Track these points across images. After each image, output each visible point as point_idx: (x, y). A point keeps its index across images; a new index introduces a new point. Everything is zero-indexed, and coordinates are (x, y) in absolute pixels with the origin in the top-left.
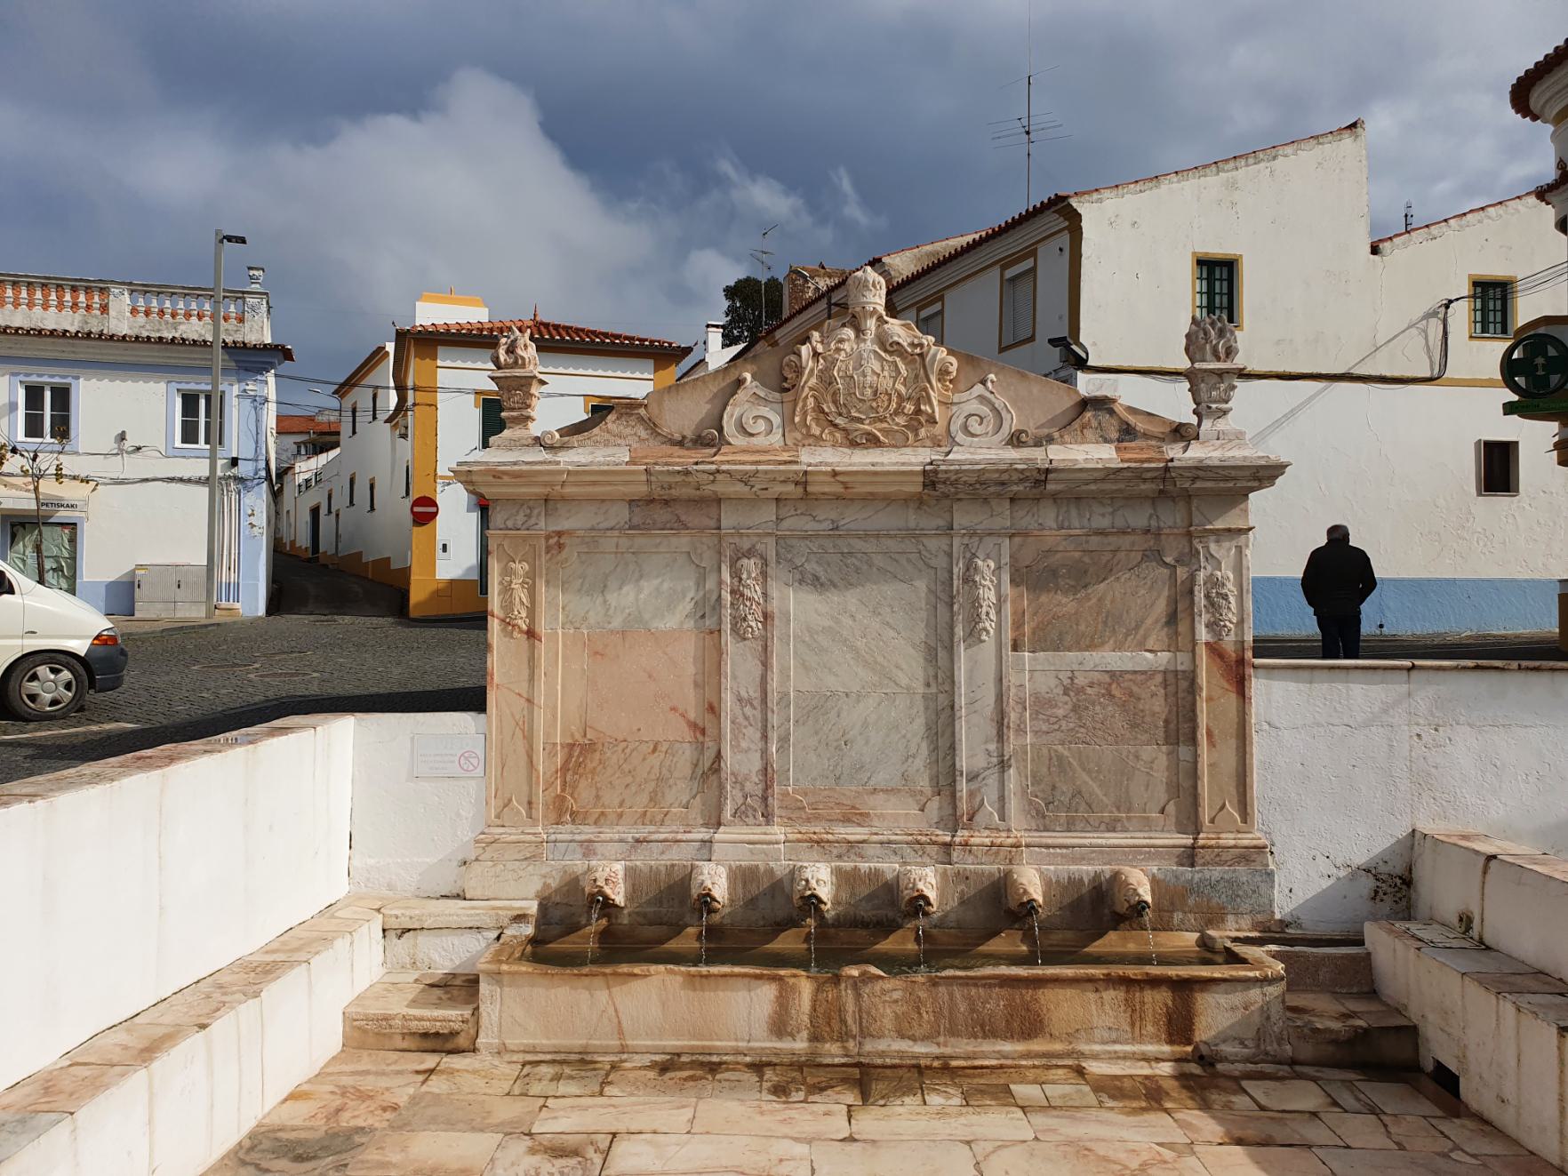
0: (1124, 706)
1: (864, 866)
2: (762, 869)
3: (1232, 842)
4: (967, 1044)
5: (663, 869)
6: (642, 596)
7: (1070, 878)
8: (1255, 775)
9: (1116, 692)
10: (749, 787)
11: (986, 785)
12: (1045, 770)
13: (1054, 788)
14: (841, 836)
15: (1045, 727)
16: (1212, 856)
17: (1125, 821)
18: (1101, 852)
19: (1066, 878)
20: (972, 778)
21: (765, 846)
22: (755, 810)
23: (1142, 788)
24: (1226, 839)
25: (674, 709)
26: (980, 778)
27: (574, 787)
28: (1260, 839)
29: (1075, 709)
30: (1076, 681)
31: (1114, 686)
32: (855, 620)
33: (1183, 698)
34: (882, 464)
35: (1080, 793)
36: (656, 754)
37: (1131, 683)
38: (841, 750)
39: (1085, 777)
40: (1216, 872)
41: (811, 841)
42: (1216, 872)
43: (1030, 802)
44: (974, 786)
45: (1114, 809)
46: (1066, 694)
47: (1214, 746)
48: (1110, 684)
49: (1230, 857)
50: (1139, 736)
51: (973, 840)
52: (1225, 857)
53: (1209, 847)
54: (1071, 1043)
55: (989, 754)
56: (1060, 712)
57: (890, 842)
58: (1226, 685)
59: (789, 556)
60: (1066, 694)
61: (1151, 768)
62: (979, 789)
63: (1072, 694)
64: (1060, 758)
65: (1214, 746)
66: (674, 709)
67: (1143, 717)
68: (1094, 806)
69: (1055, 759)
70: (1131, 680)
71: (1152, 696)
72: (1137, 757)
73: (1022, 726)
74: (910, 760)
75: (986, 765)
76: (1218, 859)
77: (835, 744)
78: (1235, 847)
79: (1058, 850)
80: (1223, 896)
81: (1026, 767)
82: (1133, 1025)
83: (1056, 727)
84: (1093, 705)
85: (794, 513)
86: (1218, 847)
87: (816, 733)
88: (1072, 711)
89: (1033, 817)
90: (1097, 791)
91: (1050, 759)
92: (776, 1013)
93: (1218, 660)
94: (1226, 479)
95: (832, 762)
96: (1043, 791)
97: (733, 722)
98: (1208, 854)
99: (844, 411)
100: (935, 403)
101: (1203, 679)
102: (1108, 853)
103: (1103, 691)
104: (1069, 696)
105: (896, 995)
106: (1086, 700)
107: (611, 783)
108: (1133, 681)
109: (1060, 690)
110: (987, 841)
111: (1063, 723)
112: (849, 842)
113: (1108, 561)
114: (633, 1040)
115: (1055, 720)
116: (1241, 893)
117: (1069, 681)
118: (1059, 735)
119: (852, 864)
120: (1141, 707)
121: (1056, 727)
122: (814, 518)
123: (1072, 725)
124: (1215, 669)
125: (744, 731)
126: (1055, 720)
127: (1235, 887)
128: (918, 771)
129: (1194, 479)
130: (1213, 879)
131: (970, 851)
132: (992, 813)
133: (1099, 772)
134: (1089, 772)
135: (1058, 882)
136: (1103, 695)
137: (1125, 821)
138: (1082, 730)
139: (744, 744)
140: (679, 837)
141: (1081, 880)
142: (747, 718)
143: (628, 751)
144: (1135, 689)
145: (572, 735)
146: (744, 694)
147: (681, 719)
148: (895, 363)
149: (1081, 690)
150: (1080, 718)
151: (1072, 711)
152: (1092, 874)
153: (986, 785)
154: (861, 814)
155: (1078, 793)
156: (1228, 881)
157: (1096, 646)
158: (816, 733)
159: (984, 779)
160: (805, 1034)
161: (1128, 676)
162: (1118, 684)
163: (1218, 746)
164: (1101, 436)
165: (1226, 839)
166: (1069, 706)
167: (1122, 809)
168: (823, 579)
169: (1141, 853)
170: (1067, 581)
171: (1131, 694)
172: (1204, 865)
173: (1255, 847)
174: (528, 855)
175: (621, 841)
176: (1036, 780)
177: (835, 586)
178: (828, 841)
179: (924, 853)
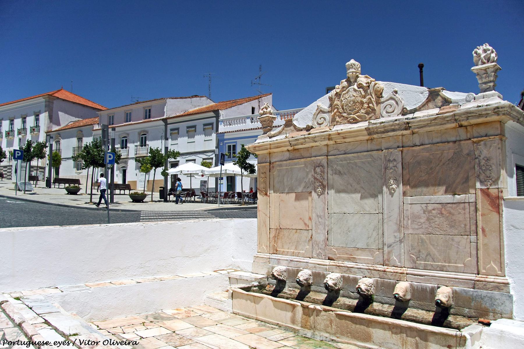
0: (447, 218)
1: (351, 276)
2: (321, 274)
3: (492, 280)
4: (346, 339)
5: (295, 270)
6: (292, 182)
7: (422, 288)
8: (505, 250)
9: (444, 212)
10: (320, 246)
11: (394, 249)
12: (416, 244)
13: (419, 251)
14: (346, 265)
15: (416, 227)
16: (482, 285)
17: (447, 267)
18: (436, 279)
19: (421, 288)
20: (389, 246)
21: (322, 266)
22: (321, 254)
23: (455, 254)
24: (490, 278)
25: (301, 219)
26: (392, 246)
27: (277, 243)
28: (507, 280)
29: (428, 219)
30: (428, 208)
31: (443, 209)
32: (352, 187)
33: (472, 214)
34: (354, 128)
35: (429, 254)
36: (297, 233)
37: (450, 208)
38: (348, 234)
39: (431, 247)
40: (484, 292)
41: (336, 266)
42: (484, 292)
43: (411, 257)
44: (390, 249)
45: (443, 262)
46: (424, 213)
47: (486, 236)
48: (441, 209)
49: (491, 287)
50: (454, 231)
51: (387, 270)
52: (488, 286)
53: (481, 281)
54: (380, 347)
55: (395, 237)
56: (422, 221)
57: (360, 268)
58: (491, 208)
59: (332, 165)
60: (424, 213)
61: (459, 245)
62: (391, 251)
63: (426, 213)
64: (422, 240)
65: (486, 236)
66: (301, 219)
67: (455, 223)
68: (435, 260)
69: (420, 240)
70: (450, 207)
71: (459, 214)
72: (453, 240)
73: (408, 226)
74: (369, 239)
75: (394, 242)
76: (485, 287)
77: (346, 232)
78: (493, 282)
79: (416, 277)
80: (487, 304)
81: (409, 243)
82: (403, 345)
83: (420, 227)
84: (435, 217)
85: (333, 149)
86: (485, 282)
87: (340, 228)
88: (427, 220)
89: (411, 263)
90: (436, 253)
91: (418, 240)
92: (292, 316)
93: (487, 197)
94: (480, 116)
95: (345, 238)
96: (416, 253)
97: (316, 223)
98: (480, 285)
99: (346, 111)
100: (374, 103)
101: (479, 206)
102: (438, 280)
103: (439, 212)
104: (425, 213)
105: (325, 317)
106: (432, 215)
107: (286, 242)
108: (451, 207)
109: (422, 212)
110: (392, 271)
111: (424, 225)
112: (348, 267)
113: (440, 157)
114: (259, 316)
115: (420, 224)
116: (496, 303)
117: (425, 208)
118: (422, 230)
119: (348, 275)
120: (454, 218)
121: (420, 227)
122: (339, 150)
123: (427, 226)
124: (486, 201)
125: (319, 226)
126: (420, 224)
127: (493, 301)
128: (372, 243)
129: (467, 118)
130: (482, 295)
131: (386, 274)
132: (395, 260)
133: (437, 246)
134: (433, 245)
135: (417, 289)
136: (439, 214)
137: (447, 267)
138: (431, 228)
139: (319, 231)
140: (301, 260)
141: (426, 289)
142: (319, 222)
143: (290, 232)
144: (452, 211)
145: (277, 226)
146: (319, 214)
147: (302, 222)
148: (360, 91)
149: (430, 212)
150: (430, 223)
151: (427, 220)
152: (431, 288)
153: (394, 249)
154: (353, 257)
155: (428, 254)
156: (489, 297)
157: (436, 193)
158: (340, 228)
159: (393, 247)
160: (300, 325)
161: (449, 205)
162: (445, 209)
163: (487, 236)
164: (435, 106)
165: (490, 278)
166: (426, 218)
167: (446, 262)
168: (342, 172)
169: (452, 281)
170: (424, 166)
171: (450, 213)
172: (478, 289)
173: (503, 283)
174: (265, 262)
175: (286, 260)
176: (413, 248)
177: (346, 174)
178: (342, 266)
179: (371, 273)
